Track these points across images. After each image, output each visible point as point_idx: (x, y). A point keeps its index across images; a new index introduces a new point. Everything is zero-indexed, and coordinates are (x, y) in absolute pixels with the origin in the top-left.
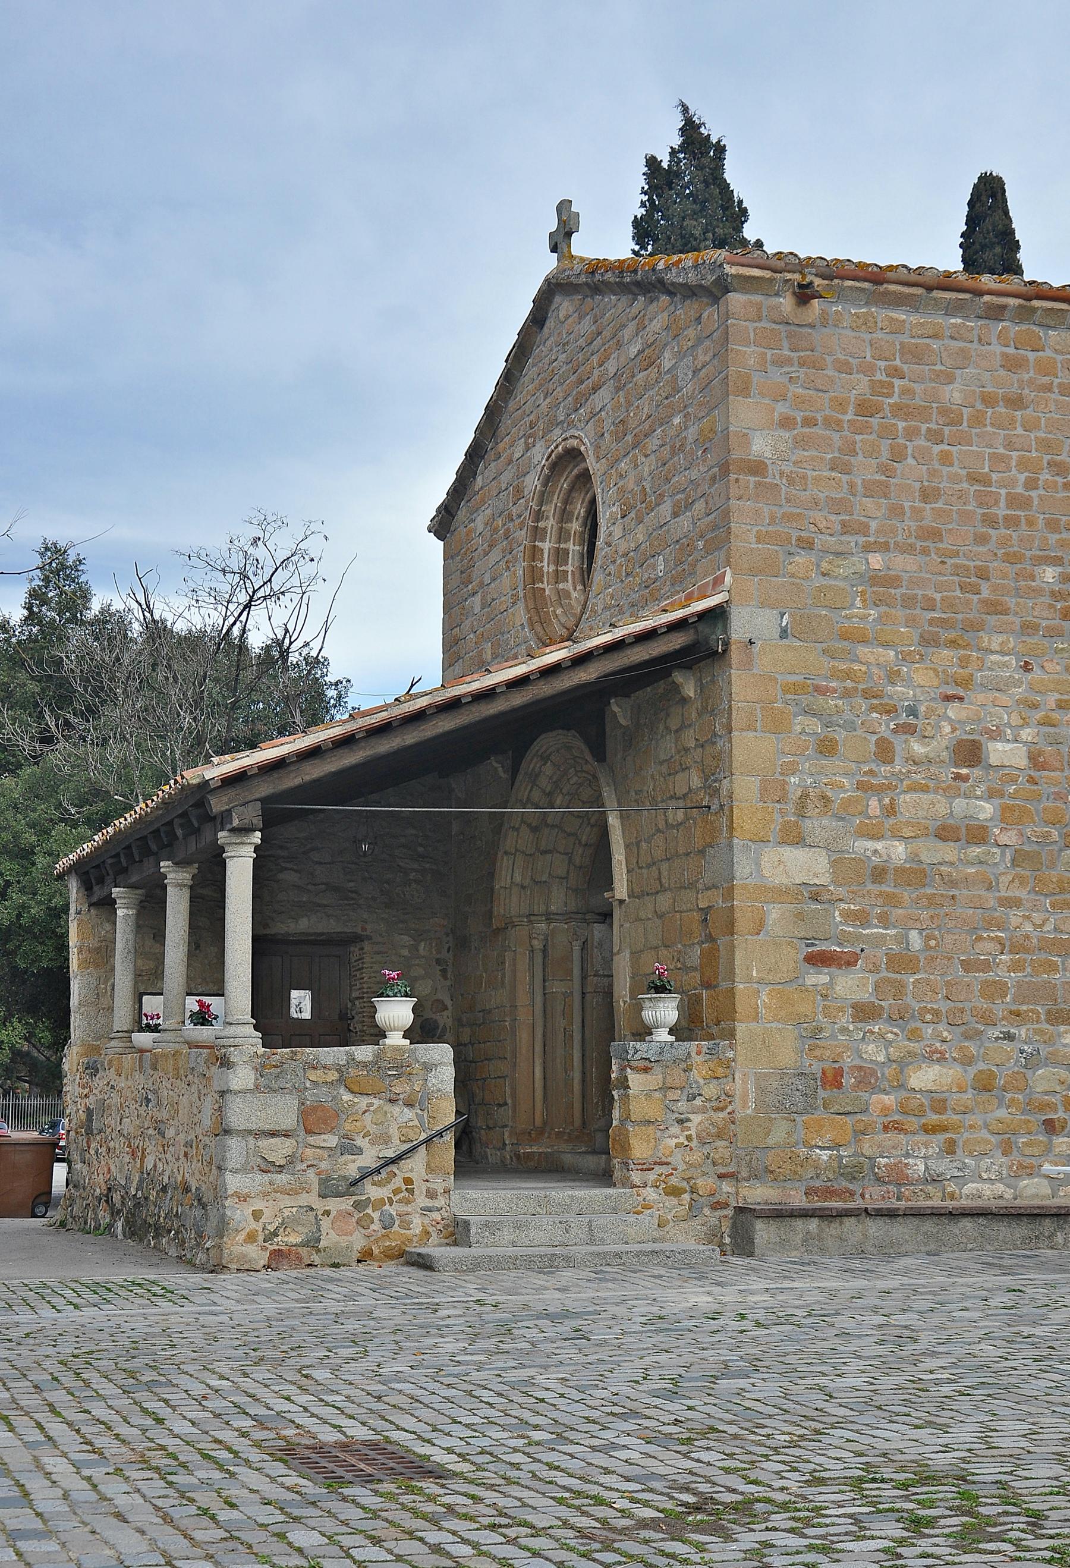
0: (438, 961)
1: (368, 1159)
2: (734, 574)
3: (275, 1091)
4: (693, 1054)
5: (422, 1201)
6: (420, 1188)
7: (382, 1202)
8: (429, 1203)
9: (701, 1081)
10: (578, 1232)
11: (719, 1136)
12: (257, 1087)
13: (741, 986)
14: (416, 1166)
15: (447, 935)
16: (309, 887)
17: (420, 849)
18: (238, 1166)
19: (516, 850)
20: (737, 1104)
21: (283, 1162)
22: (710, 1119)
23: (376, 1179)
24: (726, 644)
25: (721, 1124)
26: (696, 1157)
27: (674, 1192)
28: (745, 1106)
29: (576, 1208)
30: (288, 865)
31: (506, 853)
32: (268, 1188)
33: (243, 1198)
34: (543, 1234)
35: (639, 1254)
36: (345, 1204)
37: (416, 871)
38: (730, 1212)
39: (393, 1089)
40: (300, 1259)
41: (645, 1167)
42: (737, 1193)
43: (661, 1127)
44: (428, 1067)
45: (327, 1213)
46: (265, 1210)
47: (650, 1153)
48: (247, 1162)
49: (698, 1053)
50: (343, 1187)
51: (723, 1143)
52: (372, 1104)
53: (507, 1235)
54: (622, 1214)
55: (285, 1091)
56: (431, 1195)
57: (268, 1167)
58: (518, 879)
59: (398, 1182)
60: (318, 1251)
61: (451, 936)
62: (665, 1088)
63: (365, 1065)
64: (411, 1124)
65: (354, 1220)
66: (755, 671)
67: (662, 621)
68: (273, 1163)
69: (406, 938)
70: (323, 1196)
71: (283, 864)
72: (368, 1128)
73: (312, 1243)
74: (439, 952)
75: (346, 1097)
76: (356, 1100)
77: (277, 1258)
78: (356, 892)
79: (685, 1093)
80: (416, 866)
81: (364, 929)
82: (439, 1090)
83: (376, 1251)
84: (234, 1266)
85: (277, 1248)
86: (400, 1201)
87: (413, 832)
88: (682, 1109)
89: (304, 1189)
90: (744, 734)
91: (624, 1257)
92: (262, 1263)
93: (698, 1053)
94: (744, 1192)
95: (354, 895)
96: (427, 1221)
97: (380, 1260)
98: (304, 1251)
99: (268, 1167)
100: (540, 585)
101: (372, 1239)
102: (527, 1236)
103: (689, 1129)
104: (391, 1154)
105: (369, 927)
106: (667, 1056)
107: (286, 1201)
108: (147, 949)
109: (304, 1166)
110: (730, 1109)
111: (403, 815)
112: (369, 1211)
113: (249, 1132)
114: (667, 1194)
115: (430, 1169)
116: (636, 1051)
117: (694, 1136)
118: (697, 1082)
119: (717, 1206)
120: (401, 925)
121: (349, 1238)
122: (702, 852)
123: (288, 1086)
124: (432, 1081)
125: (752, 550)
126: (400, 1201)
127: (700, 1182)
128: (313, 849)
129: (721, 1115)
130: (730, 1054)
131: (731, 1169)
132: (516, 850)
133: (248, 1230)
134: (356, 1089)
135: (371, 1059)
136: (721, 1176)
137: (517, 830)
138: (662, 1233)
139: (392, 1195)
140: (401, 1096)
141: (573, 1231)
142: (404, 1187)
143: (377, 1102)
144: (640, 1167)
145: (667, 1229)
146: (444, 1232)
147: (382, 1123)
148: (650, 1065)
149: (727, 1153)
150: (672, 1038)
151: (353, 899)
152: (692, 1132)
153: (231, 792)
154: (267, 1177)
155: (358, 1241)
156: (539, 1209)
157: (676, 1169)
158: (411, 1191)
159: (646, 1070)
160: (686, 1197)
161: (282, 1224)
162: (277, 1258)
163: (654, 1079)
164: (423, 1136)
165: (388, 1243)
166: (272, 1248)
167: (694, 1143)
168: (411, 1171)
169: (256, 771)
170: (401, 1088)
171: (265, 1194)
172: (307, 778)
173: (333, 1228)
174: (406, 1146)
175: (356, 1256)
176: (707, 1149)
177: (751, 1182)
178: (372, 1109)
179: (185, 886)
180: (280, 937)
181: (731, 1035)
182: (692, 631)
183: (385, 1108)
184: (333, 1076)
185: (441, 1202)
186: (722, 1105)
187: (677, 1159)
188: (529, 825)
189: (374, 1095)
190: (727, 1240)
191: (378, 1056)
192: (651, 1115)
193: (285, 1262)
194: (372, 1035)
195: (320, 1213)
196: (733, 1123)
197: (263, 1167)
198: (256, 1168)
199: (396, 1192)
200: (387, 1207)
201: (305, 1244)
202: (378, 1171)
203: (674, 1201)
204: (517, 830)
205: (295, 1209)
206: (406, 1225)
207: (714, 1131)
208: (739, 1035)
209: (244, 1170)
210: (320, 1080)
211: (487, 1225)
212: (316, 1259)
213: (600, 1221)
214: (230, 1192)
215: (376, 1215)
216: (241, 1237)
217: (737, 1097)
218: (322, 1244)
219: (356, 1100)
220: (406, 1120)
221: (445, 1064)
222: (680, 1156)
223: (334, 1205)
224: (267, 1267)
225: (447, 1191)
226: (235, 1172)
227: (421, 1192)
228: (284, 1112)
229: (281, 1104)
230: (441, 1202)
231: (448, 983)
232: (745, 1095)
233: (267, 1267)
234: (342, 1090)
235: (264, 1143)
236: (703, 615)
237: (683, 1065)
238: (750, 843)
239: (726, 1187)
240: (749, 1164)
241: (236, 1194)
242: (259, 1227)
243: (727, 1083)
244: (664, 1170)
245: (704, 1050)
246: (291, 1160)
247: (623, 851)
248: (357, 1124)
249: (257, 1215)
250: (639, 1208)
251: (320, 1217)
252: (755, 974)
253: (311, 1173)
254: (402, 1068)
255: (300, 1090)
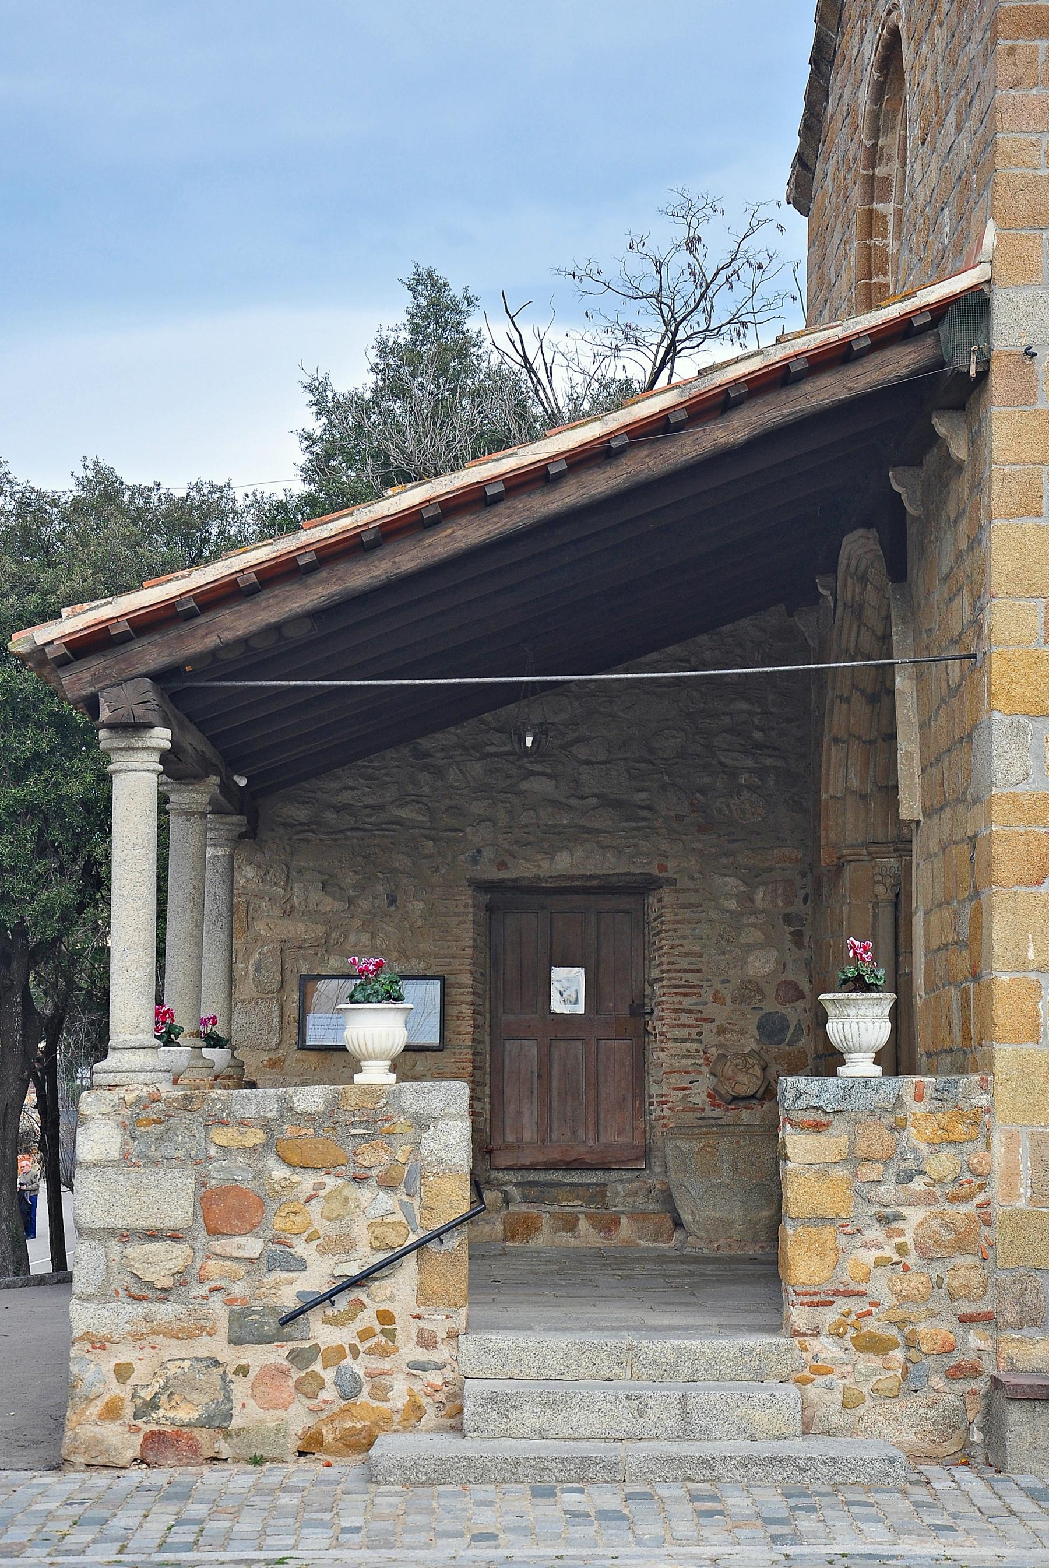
0: (787, 919)
1: (316, 1278)
2: (1001, 227)
3: (156, 1164)
4: (908, 1099)
5: (409, 1351)
6: (406, 1330)
7: (338, 1353)
8: (422, 1355)
9: (924, 1149)
10: (661, 1415)
11: (960, 1246)
12: (125, 1156)
13: (1004, 978)
14: (400, 1290)
15: (804, 875)
16: (573, 802)
17: (758, 735)
18: (92, 1290)
19: (850, 735)
20: (996, 1190)
21: (167, 1283)
22: (941, 1215)
23: (330, 1312)
24: (985, 363)
25: (962, 1225)
26: (915, 1283)
27: (875, 1345)
28: (1011, 1193)
29: (685, 1369)
30: (537, 767)
31: (836, 740)
32: (142, 1327)
33: (100, 1344)
34: (593, 1418)
35: (745, 1463)
36: (276, 1355)
37: (749, 770)
38: (981, 1385)
39: (360, 1159)
40: (194, 1448)
41: (816, 1299)
42: (997, 1352)
43: (848, 1229)
44: (421, 1123)
45: (243, 1370)
46: (138, 1366)
47: (826, 1274)
48: (106, 1283)
49: (919, 1098)
50: (271, 1325)
51: (969, 1260)
52: (322, 1186)
53: (529, 1417)
54: (771, 1382)
55: (174, 1162)
56: (426, 1341)
57: (143, 1292)
58: (855, 783)
59: (367, 1318)
60: (228, 1435)
61: (809, 875)
62: (853, 1160)
63: (311, 1118)
64: (390, 1219)
65: (291, 1383)
66: (1039, 406)
67: (859, 328)
68: (150, 1285)
69: (732, 881)
70: (236, 1341)
71: (530, 767)
72: (316, 1226)
73: (218, 1420)
74: (789, 903)
75: (279, 1172)
76: (295, 1178)
77: (156, 1447)
78: (649, 808)
79: (893, 1168)
80: (750, 763)
81: (662, 868)
82: (441, 1161)
83: (329, 1437)
84: (80, 1459)
85: (156, 1428)
86: (370, 1352)
87: (743, 706)
88: (887, 1197)
89: (203, 1328)
90: (1017, 522)
91: (719, 1468)
92: (130, 1454)
93: (919, 1098)
94: (1011, 1349)
95: (645, 813)
96: (418, 1387)
97: (337, 1453)
98: (203, 1436)
99: (143, 1292)
100: (881, 279)
101: (323, 1415)
102: (566, 1420)
103: (901, 1233)
104: (353, 1270)
105: (671, 864)
106: (858, 1103)
107: (173, 1348)
108: (312, 907)
109: (204, 1290)
110: (980, 1198)
111: (728, 680)
112: (317, 1367)
113: (111, 1232)
114: (861, 1348)
115: (423, 1297)
116: (799, 1095)
117: (911, 1246)
118: (914, 1150)
119: (955, 1373)
120: (724, 860)
121: (282, 1413)
122: (970, 736)
123: (178, 1154)
124: (430, 1145)
125: (1037, 180)
126: (370, 1352)
127: (923, 1328)
128: (576, 741)
129: (964, 1209)
130: (983, 1100)
131: (984, 1307)
132: (850, 735)
133: (106, 1398)
134: (295, 1159)
135: (321, 1108)
136: (966, 1320)
137: (848, 700)
138: (848, 1419)
139: (356, 1341)
140: (374, 1172)
141: (652, 1414)
142: (378, 1327)
143: (331, 1182)
144: (807, 1299)
145: (859, 1411)
146: (449, 1405)
147: (339, 1217)
148: (824, 1119)
149: (975, 1278)
150: (878, 1070)
151: (644, 819)
152: (908, 1239)
153: (96, 665)
154: (140, 1308)
155: (298, 1419)
156: (617, 1370)
157: (876, 1305)
158: (391, 1335)
159: (818, 1127)
160: (898, 1355)
161: (165, 1387)
162: (156, 1447)
163: (833, 1143)
164: (413, 1238)
165: (349, 1424)
166: (147, 1428)
167: (912, 1259)
168: (391, 1299)
169: (124, 627)
170: (371, 1157)
171: (138, 1338)
172: (227, 636)
173: (253, 1396)
174: (381, 1257)
175: (294, 1444)
176: (935, 1270)
177: (1026, 1331)
178: (322, 1193)
179: (193, 814)
180: (524, 883)
181: (984, 1066)
182: (930, 341)
183: (345, 1192)
184: (255, 1137)
185: (442, 1353)
186: (965, 1190)
187: (880, 1287)
188: (863, 692)
189: (327, 1169)
190: (977, 1436)
191: (334, 1105)
192: (827, 1206)
193: (170, 1453)
194: (675, 1040)
195: (230, 1370)
196: (987, 1223)
197: (135, 1290)
198: (122, 1293)
199: (365, 1335)
200: (348, 1361)
201: (205, 1422)
202: (329, 1297)
203: (877, 1361)
204: (848, 700)
205: (187, 1364)
206: (381, 1392)
207: (948, 1237)
208: (999, 1065)
209: (102, 1295)
210: (234, 1145)
211: (493, 1399)
212: (225, 1449)
213: (704, 1396)
214: (77, 1333)
215: (329, 1376)
216: (95, 1409)
217: (996, 1178)
218: (235, 1423)
219: (295, 1178)
220: (381, 1212)
221: (452, 1117)
222: (884, 1281)
223: (256, 1356)
224: (140, 1460)
225: (453, 1335)
226: (86, 1298)
227: (409, 1337)
228: (172, 1199)
229: (165, 1185)
230: (442, 1353)
231: (806, 954)
232: (1011, 1177)
233: (140, 1460)
234: (272, 1162)
235: (136, 1251)
236: (941, 311)
237: (888, 1120)
238: (1023, 720)
239: (976, 1339)
240: (1020, 1299)
241: (87, 1337)
242: (123, 1392)
243: (974, 1152)
244: (855, 1305)
245: (929, 1092)
246: (183, 1279)
247: (916, 734)
248: (298, 1219)
249: (123, 1372)
250: (807, 1373)
251: (231, 1377)
252: (1031, 955)
253: (217, 1300)
254: (376, 1123)
255: (200, 1161)
